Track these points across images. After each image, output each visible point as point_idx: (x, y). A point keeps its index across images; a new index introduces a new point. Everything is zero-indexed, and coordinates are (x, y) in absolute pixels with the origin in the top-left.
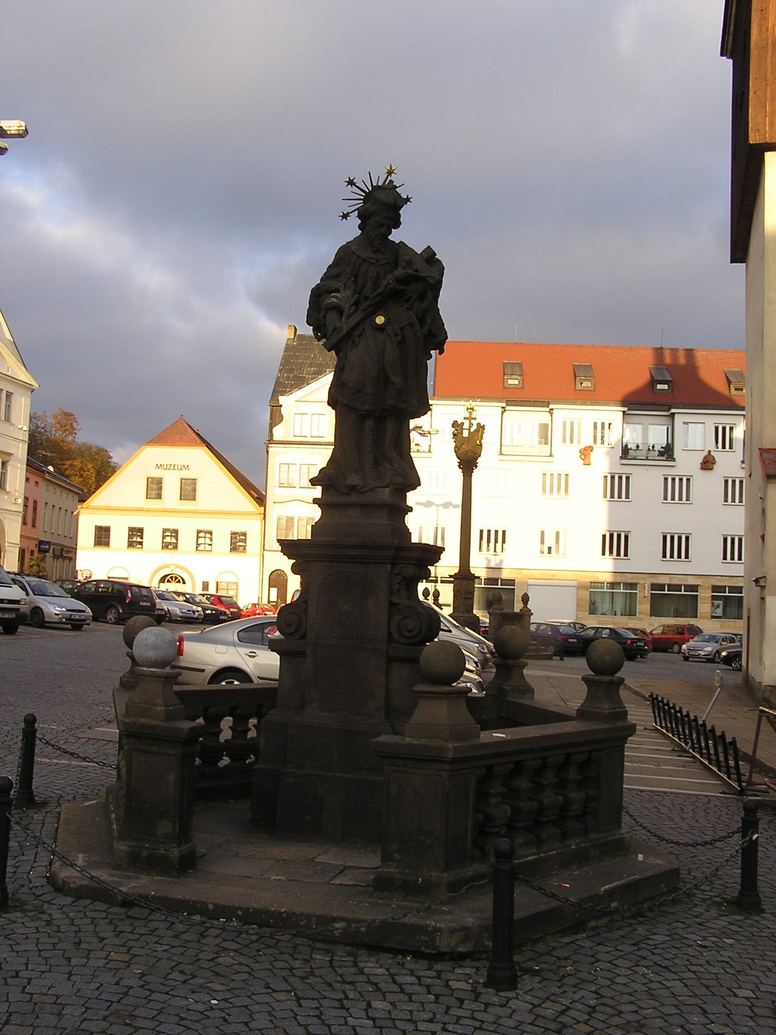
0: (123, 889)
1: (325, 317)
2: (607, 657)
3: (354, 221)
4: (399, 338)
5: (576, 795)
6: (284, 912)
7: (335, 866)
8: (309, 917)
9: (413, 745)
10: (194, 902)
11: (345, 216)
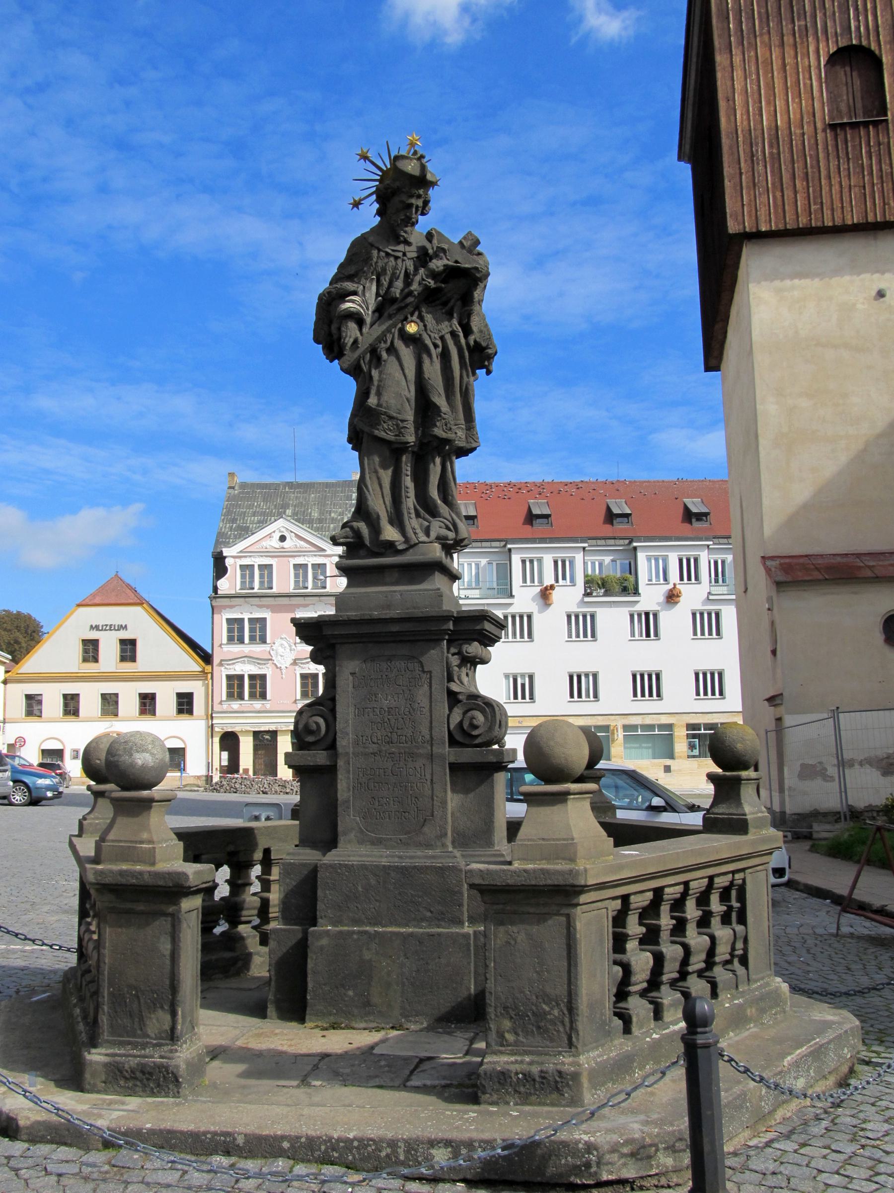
0: (100, 1123)
1: (339, 329)
2: (739, 746)
3: (371, 207)
4: (440, 350)
5: (723, 933)
6: (355, 1139)
7: (406, 1059)
8: (393, 1144)
9: (525, 871)
10: (215, 1134)
11: (356, 204)
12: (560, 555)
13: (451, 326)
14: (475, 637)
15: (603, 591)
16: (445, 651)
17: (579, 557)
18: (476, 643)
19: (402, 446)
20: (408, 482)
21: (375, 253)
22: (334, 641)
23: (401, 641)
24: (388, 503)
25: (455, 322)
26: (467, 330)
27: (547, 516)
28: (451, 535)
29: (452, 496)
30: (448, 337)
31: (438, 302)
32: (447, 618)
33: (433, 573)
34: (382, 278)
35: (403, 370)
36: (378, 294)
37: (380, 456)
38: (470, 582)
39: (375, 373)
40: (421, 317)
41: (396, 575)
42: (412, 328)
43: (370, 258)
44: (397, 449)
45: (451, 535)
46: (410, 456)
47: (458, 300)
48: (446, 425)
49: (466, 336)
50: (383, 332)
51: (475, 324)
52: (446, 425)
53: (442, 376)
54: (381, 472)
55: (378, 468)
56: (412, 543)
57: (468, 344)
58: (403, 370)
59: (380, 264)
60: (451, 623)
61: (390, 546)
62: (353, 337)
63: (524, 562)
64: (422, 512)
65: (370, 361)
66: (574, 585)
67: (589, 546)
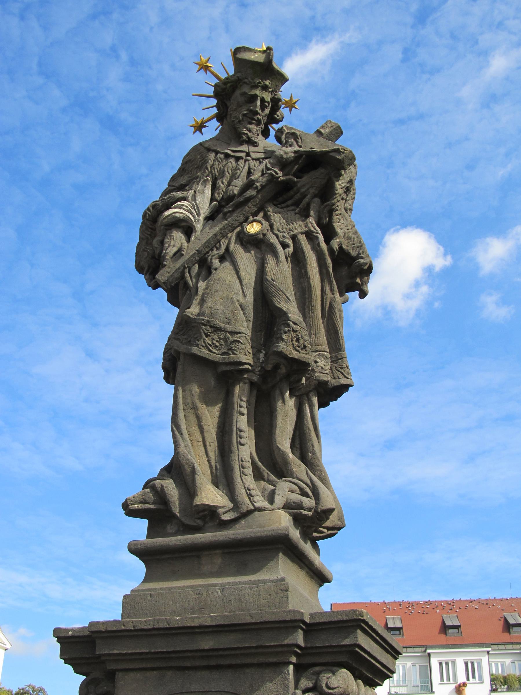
1: (162, 243)
4: (291, 249)
12: (469, 658)
13: (306, 226)
14: (343, 658)
15: (506, 687)
16: (292, 684)
17: (485, 659)
18: (345, 670)
19: (231, 368)
20: (242, 422)
21: (212, 156)
22: (112, 666)
23: (218, 667)
24: (212, 455)
25: (312, 220)
26: (329, 233)
27: (457, 627)
28: (308, 502)
29: (314, 453)
30: (303, 239)
31: (289, 202)
32: (293, 624)
33: (274, 556)
34: (219, 182)
35: (237, 272)
36: (212, 199)
37: (199, 387)
38: (398, 681)
39: (202, 285)
40: (267, 218)
41: (218, 561)
42: (253, 228)
43: (205, 161)
44: (225, 373)
45: (308, 502)
46: (247, 387)
47: (315, 196)
48: (298, 340)
49: (328, 241)
50: (215, 235)
51: (339, 226)
52: (298, 340)
53: (294, 286)
54: (203, 409)
55: (197, 401)
56: (244, 509)
57: (331, 250)
58: (237, 272)
59: (217, 166)
60: (300, 632)
61: (209, 515)
62: (178, 245)
63: (441, 664)
64: (266, 472)
65: (198, 275)
66: (483, 683)
67: (492, 650)
